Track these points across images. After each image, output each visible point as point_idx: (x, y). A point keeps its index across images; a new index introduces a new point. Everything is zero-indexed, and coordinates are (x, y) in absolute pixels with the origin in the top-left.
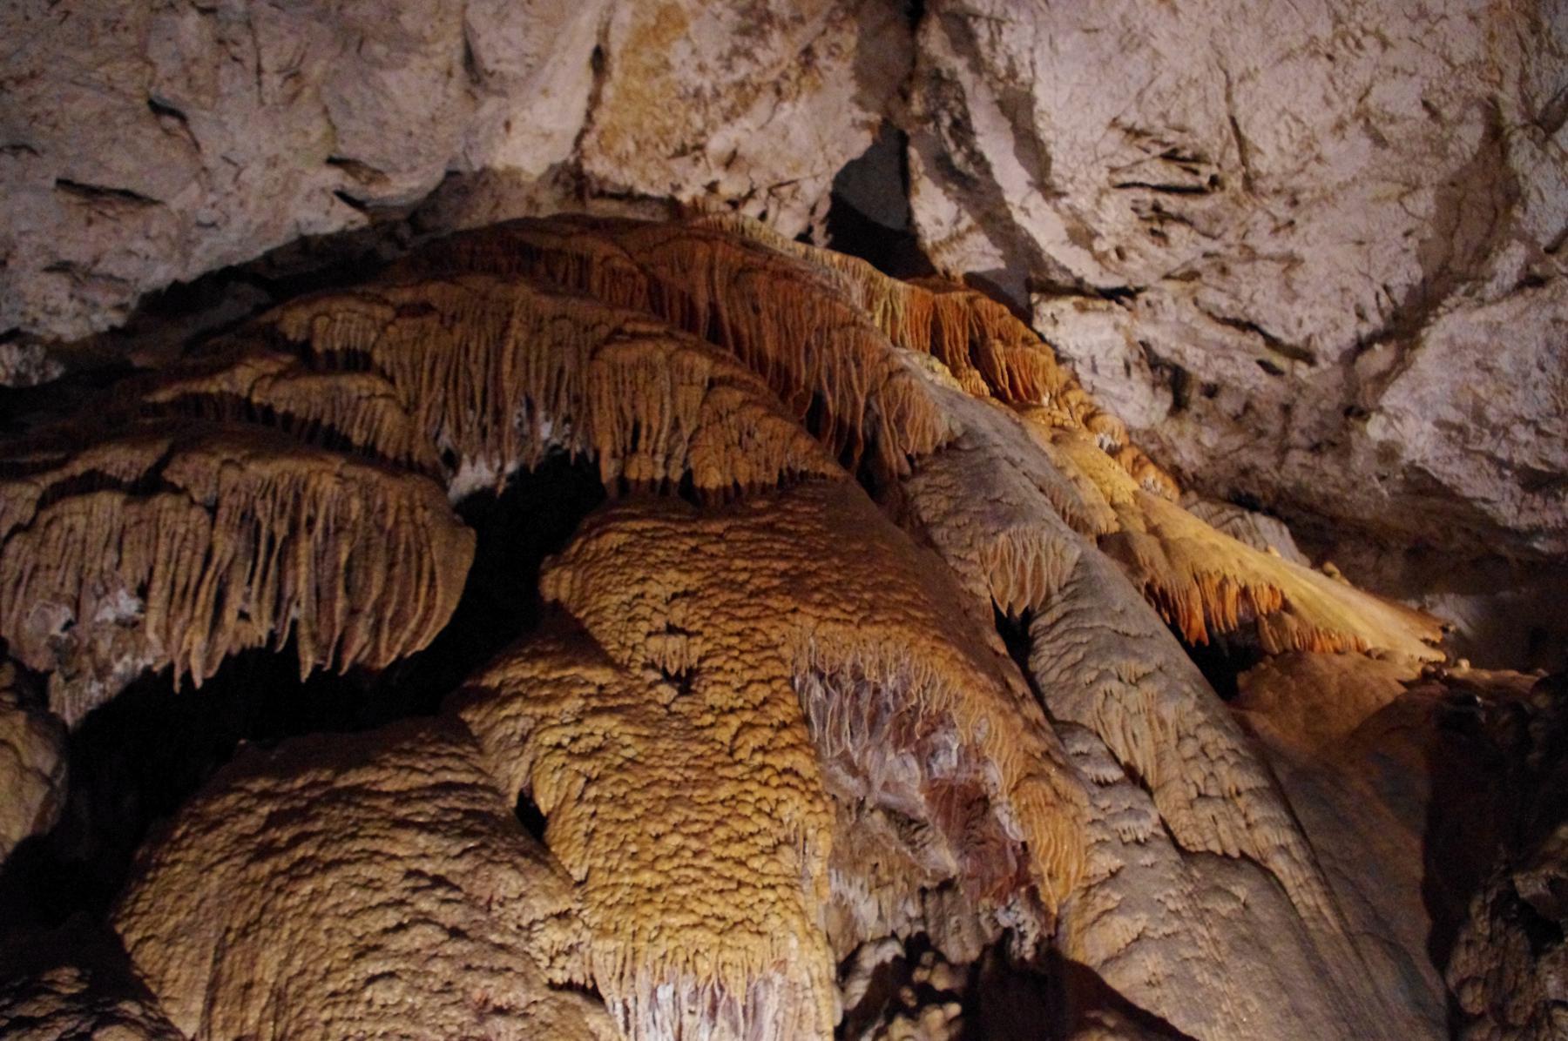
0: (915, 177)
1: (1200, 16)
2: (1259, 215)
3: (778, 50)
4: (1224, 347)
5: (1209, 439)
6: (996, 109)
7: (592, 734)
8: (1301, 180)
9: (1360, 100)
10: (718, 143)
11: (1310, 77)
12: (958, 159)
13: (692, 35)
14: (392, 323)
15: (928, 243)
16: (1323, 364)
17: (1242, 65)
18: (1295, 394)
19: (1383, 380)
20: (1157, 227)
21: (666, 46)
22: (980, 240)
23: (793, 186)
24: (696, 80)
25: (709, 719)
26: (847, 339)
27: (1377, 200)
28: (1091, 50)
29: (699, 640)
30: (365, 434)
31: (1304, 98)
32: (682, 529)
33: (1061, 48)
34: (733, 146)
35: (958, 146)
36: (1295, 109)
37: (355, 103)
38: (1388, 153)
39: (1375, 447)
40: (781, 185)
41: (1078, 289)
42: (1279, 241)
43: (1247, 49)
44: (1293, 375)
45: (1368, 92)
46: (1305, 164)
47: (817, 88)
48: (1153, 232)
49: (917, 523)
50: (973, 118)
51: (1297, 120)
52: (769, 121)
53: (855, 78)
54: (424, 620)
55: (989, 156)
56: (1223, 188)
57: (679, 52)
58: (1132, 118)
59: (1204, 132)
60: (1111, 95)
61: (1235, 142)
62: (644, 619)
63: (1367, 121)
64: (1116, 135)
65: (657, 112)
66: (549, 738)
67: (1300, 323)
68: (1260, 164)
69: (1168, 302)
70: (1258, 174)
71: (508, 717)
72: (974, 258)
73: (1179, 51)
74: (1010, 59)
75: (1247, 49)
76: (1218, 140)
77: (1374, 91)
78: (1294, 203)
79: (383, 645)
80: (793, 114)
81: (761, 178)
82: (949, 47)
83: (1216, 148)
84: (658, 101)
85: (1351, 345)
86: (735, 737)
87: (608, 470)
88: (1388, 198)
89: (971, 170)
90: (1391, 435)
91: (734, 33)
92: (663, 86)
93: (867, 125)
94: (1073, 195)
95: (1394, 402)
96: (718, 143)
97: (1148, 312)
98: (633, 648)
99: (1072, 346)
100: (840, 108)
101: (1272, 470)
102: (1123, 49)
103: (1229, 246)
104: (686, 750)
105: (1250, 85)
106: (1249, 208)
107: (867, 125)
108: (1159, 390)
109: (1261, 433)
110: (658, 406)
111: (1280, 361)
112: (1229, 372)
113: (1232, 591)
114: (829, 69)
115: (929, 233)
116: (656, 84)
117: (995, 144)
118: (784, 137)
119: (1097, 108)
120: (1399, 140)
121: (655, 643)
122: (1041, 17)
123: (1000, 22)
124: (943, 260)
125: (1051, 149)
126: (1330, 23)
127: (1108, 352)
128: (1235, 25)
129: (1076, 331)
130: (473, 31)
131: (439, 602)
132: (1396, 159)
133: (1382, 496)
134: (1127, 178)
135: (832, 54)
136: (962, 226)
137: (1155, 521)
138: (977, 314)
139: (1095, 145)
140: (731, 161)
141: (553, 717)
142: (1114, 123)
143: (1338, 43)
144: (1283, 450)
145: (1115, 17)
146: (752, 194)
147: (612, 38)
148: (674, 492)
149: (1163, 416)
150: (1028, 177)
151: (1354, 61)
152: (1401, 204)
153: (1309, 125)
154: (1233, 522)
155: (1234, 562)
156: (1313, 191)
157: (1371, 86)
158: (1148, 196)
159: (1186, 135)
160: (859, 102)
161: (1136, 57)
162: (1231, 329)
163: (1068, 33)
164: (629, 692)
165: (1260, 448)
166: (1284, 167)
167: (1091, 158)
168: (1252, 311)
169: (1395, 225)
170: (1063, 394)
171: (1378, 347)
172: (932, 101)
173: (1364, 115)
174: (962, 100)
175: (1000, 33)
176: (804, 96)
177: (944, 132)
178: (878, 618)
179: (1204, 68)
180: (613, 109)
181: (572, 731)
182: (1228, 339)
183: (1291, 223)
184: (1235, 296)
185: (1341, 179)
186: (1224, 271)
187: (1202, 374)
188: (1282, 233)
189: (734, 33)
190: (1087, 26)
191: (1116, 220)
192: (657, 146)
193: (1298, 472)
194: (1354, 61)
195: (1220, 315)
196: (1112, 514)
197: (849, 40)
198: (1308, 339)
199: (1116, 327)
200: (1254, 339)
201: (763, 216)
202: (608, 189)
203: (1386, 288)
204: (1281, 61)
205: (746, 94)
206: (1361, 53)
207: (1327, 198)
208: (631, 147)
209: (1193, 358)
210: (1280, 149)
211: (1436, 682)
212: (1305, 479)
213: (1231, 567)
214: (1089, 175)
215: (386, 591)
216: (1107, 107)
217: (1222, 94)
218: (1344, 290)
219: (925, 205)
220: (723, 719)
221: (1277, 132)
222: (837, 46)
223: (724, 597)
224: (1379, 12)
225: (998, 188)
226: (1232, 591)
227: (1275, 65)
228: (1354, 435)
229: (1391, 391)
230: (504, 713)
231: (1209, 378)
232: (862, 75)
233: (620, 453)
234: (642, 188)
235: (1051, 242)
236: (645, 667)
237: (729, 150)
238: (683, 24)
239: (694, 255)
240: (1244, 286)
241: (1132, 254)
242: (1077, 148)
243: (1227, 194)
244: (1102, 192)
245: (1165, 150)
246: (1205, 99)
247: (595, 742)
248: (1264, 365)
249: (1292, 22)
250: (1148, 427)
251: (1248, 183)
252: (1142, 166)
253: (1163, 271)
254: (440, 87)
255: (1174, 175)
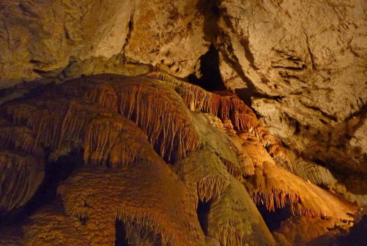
0: (221, 61)
1: (298, 18)
2: (318, 76)
3: (180, 23)
4: (309, 115)
5: (306, 141)
6: (240, 43)
7: (52, 235)
8: (331, 67)
9: (348, 43)
10: (163, 49)
11: (332, 37)
12: (230, 57)
13: (156, 19)
14: (35, 111)
15: (224, 80)
16: (340, 121)
17: (311, 33)
18: (331, 130)
19: (356, 128)
20: (286, 79)
21: (149, 22)
22: (239, 79)
23: (186, 62)
24: (157, 31)
25: (86, 233)
26: (173, 116)
27: (357, 72)
28: (266, 28)
29: (91, 209)
30: (19, 143)
31: (331, 42)
32: (97, 176)
33: (256, 27)
34: (168, 50)
35: (230, 53)
36: (327, 46)
37: (37, 47)
38: (359, 59)
39: (353, 148)
40: (182, 61)
41: (266, 97)
42: (325, 84)
43: (312, 28)
44: (330, 124)
45: (351, 41)
46: (331, 62)
47: (193, 34)
48: (286, 81)
49: (182, 173)
50: (233, 46)
51: (329, 49)
52: (179, 43)
53: (203, 32)
54: (23, 197)
55: (238, 57)
56: (306, 69)
57: (153, 23)
58: (278, 47)
59: (299, 52)
60: (272, 41)
61: (309, 55)
62: (79, 202)
63: (351, 49)
64: (273, 52)
65: (146, 40)
66: (40, 236)
67: (333, 108)
68: (316, 62)
69: (291, 100)
70: (317, 64)
71: (32, 228)
72: (238, 85)
73: (292, 29)
74: (242, 30)
75: (312, 28)
76: (304, 55)
77: (353, 41)
78: (329, 73)
79: (10, 204)
80: (186, 41)
81: (176, 59)
82: (226, 25)
83: (304, 57)
84: (147, 37)
85: (348, 116)
86: (92, 238)
87: (86, 156)
88: (360, 72)
89: (234, 60)
90: (358, 145)
91: (168, 18)
92: (148, 33)
93: (206, 45)
94: (261, 69)
95: (358, 135)
96: (163, 49)
97: (285, 104)
98: (73, 211)
99: (263, 113)
100: (199, 40)
101: (325, 153)
102: (275, 28)
103: (309, 85)
104: (77, 242)
105: (313, 39)
106: (315, 74)
107: (206, 45)
108: (291, 126)
109: (323, 141)
110: (104, 137)
111: (326, 120)
112: (311, 123)
113: (284, 195)
114: (196, 29)
115: (224, 77)
116: (146, 32)
117: (240, 54)
118: (183, 48)
119: (268, 45)
120: (362, 55)
121: (79, 209)
122: (251, 18)
123: (238, 19)
124: (230, 85)
125: (254, 56)
126: (338, 21)
127: (274, 115)
128: (309, 21)
129: (264, 108)
130: (67, 30)
131: (28, 193)
132: (362, 60)
133: (357, 163)
134: (277, 65)
135: (196, 25)
136: (234, 75)
137: (266, 172)
138: (233, 103)
139: (267, 55)
140: (168, 54)
141: (43, 230)
142: (273, 49)
143: (341, 27)
144: (328, 146)
145: (273, 19)
146: (174, 64)
147: (134, 19)
148: (104, 163)
149: (292, 134)
150: (249, 63)
151: (347, 32)
152: (365, 74)
153: (332, 51)
154: (311, 168)
155: (286, 187)
156: (335, 70)
157: (352, 39)
158: (283, 70)
159: (294, 53)
160: (204, 38)
161: (279, 30)
162: (311, 110)
163: (258, 23)
164: (66, 224)
165: (321, 146)
166: (325, 62)
167: (266, 59)
168: (317, 105)
169: (362, 80)
170: (256, 128)
171: (354, 118)
172: (222, 40)
173: (349, 47)
174: (230, 40)
175: (239, 22)
176: (189, 36)
177: (226, 49)
178: (145, 205)
179: (299, 33)
180: (134, 39)
181: (46, 234)
182: (310, 113)
183: (329, 79)
184: (312, 100)
185: (344, 66)
186: (309, 92)
187: (303, 123)
188: (326, 82)
189: (168, 18)
190: (264, 21)
191: (274, 77)
192: (146, 50)
193: (332, 154)
194: (347, 32)
195: (308, 105)
196: (254, 169)
197: (202, 21)
198: (335, 114)
199: (276, 108)
200: (318, 113)
201: (178, 70)
202: (132, 61)
203: (361, 99)
204: (323, 31)
205: (170, 37)
206: (348, 30)
207: (338, 72)
208: (139, 50)
209: (299, 117)
210: (323, 58)
211: (337, 229)
212: (335, 156)
213: (285, 188)
214: (265, 64)
215: (13, 189)
216: (271, 44)
217: (305, 41)
218: (347, 99)
219: (223, 69)
220: (90, 233)
221: (322, 52)
222: (198, 22)
223: (102, 197)
224: (353, 18)
225: (241, 66)
226: (284, 195)
227: (321, 33)
228: (347, 144)
229: (357, 132)
230: (32, 227)
231: (305, 124)
232: (205, 30)
233: (91, 151)
234: (141, 61)
235: (256, 82)
236: (75, 216)
237: (168, 51)
238: (154, 15)
239: (132, 90)
240: (315, 97)
241: (280, 87)
242: (262, 56)
243: (307, 70)
244: (269, 69)
245: (289, 57)
246: (300, 43)
247: (52, 237)
248: (322, 121)
249: (326, 20)
250: (287, 137)
251: (314, 67)
252: (281, 62)
253: (290, 92)
254: (60, 44)
255: (291, 64)
